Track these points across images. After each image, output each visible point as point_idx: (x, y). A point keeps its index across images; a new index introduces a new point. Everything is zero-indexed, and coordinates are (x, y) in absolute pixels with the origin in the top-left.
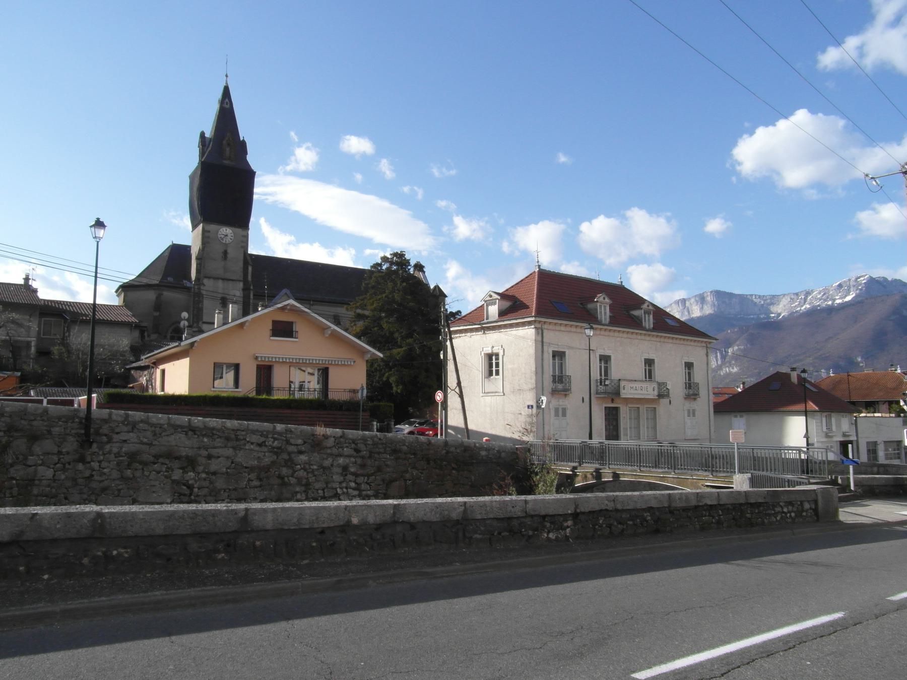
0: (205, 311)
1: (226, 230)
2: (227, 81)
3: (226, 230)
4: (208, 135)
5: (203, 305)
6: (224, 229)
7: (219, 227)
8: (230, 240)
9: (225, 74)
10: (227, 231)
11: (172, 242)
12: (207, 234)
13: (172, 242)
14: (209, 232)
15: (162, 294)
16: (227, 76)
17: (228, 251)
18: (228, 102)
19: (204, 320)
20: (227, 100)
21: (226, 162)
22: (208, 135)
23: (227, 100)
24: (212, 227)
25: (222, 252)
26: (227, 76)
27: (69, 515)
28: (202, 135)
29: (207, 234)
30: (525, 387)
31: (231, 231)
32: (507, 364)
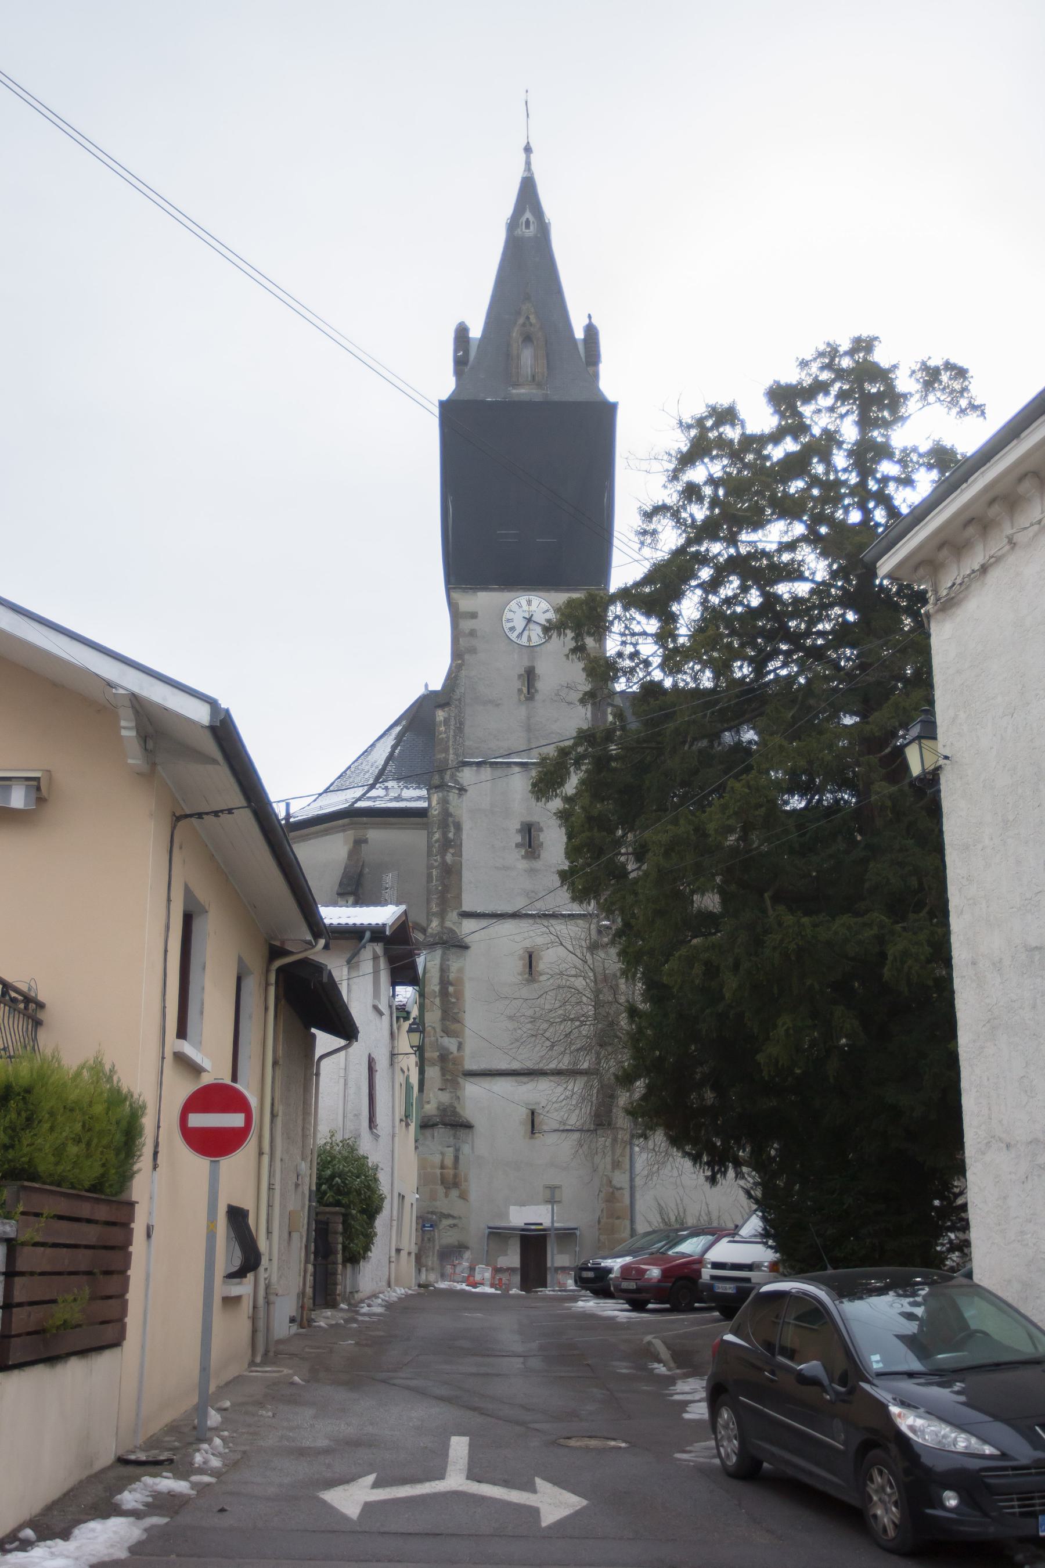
0: (467, 875)
1: (529, 603)
2: (528, 163)
3: (529, 603)
4: (476, 332)
5: (459, 854)
6: (523, 599)
7: (507, 595)
8: (510, 625)
9: (524, 144)
10: (533, 607)
11: (426, 686)
12: (466, 625)
13: (426, 686)
14: (474, 615)
15: (366, 841)
16: (528, 150)
17: (538, 671)
18: (532, 219)
19: (466, 907)
20: (528, 215)
21: (523, 392)
22: (476, 332)
23: (528, 215)
24: (482, 600)
25: (520, 676)
26: (528, 150)
27: (703, 1317)
28: (461, 334)
29: (466, 625)
30: (567, 902)
31: (545, 605)
32: (550, 1120)
